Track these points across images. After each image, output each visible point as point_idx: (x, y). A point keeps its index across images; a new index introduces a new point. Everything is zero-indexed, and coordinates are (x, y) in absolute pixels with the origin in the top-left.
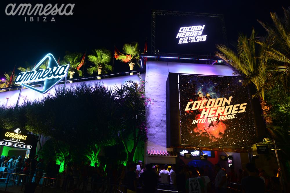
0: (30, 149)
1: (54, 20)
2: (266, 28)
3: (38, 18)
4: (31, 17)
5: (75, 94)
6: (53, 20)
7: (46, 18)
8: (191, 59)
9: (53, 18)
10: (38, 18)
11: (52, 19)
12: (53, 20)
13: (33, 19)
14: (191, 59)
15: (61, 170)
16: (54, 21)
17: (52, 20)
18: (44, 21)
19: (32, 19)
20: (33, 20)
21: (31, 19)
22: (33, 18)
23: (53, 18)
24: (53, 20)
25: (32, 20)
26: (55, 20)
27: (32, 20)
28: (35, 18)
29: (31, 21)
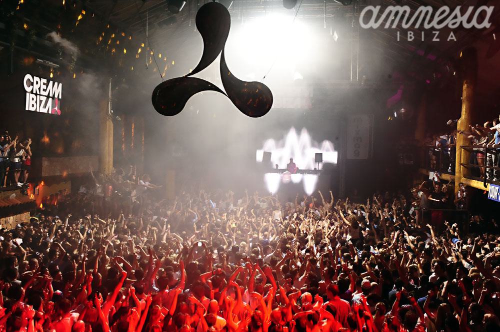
0: (315, 172)
1: (454, 38)
2: (181, 244)
3: (423, 33)
4: (409, 32)
5: (214, 205)
6: (452, 37)
7: (437, 33)
8: (435, 200)
9: (452, 34)
10: (423, 33)
11: (454, 35)
12: (452, 37)
13: (413, 35)
14: (435, 200)
15: (455, 40)
16: (453, 40)
17: (449, 38)
18: (434, 40)
19: (412, 35)
20: (413, 38)
21: (409, 35)
22: (412, 33)
23: (452, 34)
24: (452, 38)
25: (411, 38)
26: (456, 38)
27: (410, 34)
28: (417, 33)
29: (409, 40)
